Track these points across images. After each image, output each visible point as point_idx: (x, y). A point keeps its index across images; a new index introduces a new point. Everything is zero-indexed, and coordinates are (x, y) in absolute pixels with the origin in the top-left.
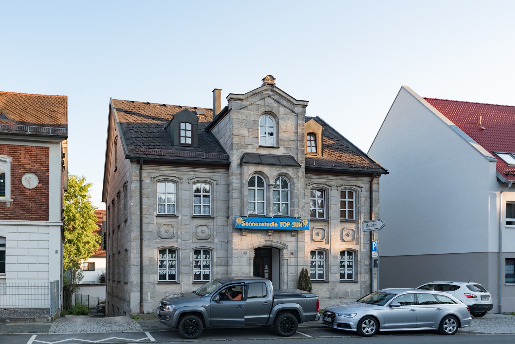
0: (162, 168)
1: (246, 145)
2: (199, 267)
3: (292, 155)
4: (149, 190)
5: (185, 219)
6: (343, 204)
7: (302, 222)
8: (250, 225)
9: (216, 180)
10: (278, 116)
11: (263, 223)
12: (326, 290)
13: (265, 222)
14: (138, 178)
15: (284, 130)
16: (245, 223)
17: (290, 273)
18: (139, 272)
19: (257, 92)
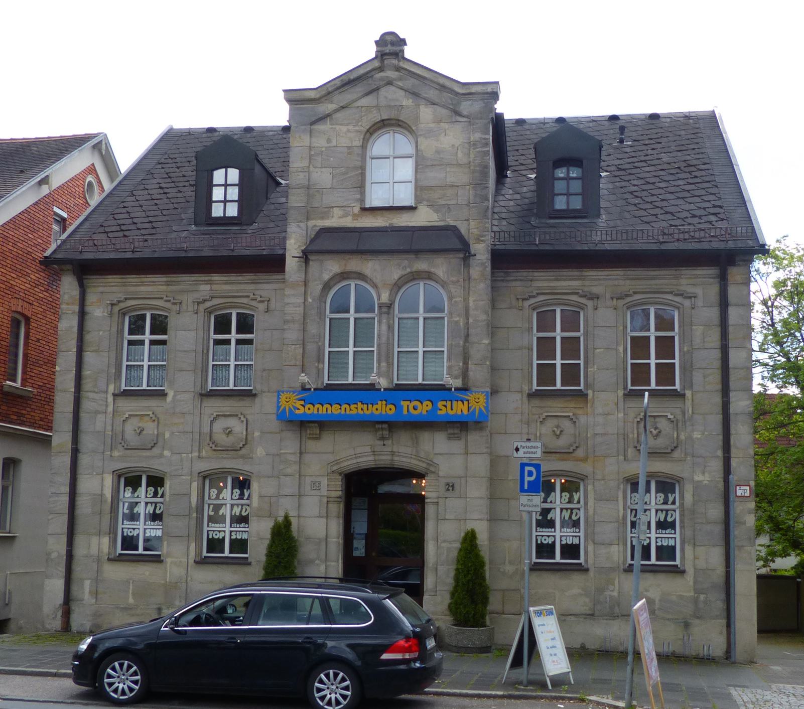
0: (133, 279)
1: (326, 210)
2: (222, 520)
3: (452, 223)
4: (101, 333)
5: (183, 401)
6: (546, 347)
7: (468, 401)
8: (316, 412)
9: (690, 298)
10: (414, 128)
11: (353, 406)
12: (580, 591)
13: (359, 404)
14: (76, 308)
15: (429, 163)
16: (304, 406)
17: (445, 541)
18: (65, 529)
19: (352, 78)
